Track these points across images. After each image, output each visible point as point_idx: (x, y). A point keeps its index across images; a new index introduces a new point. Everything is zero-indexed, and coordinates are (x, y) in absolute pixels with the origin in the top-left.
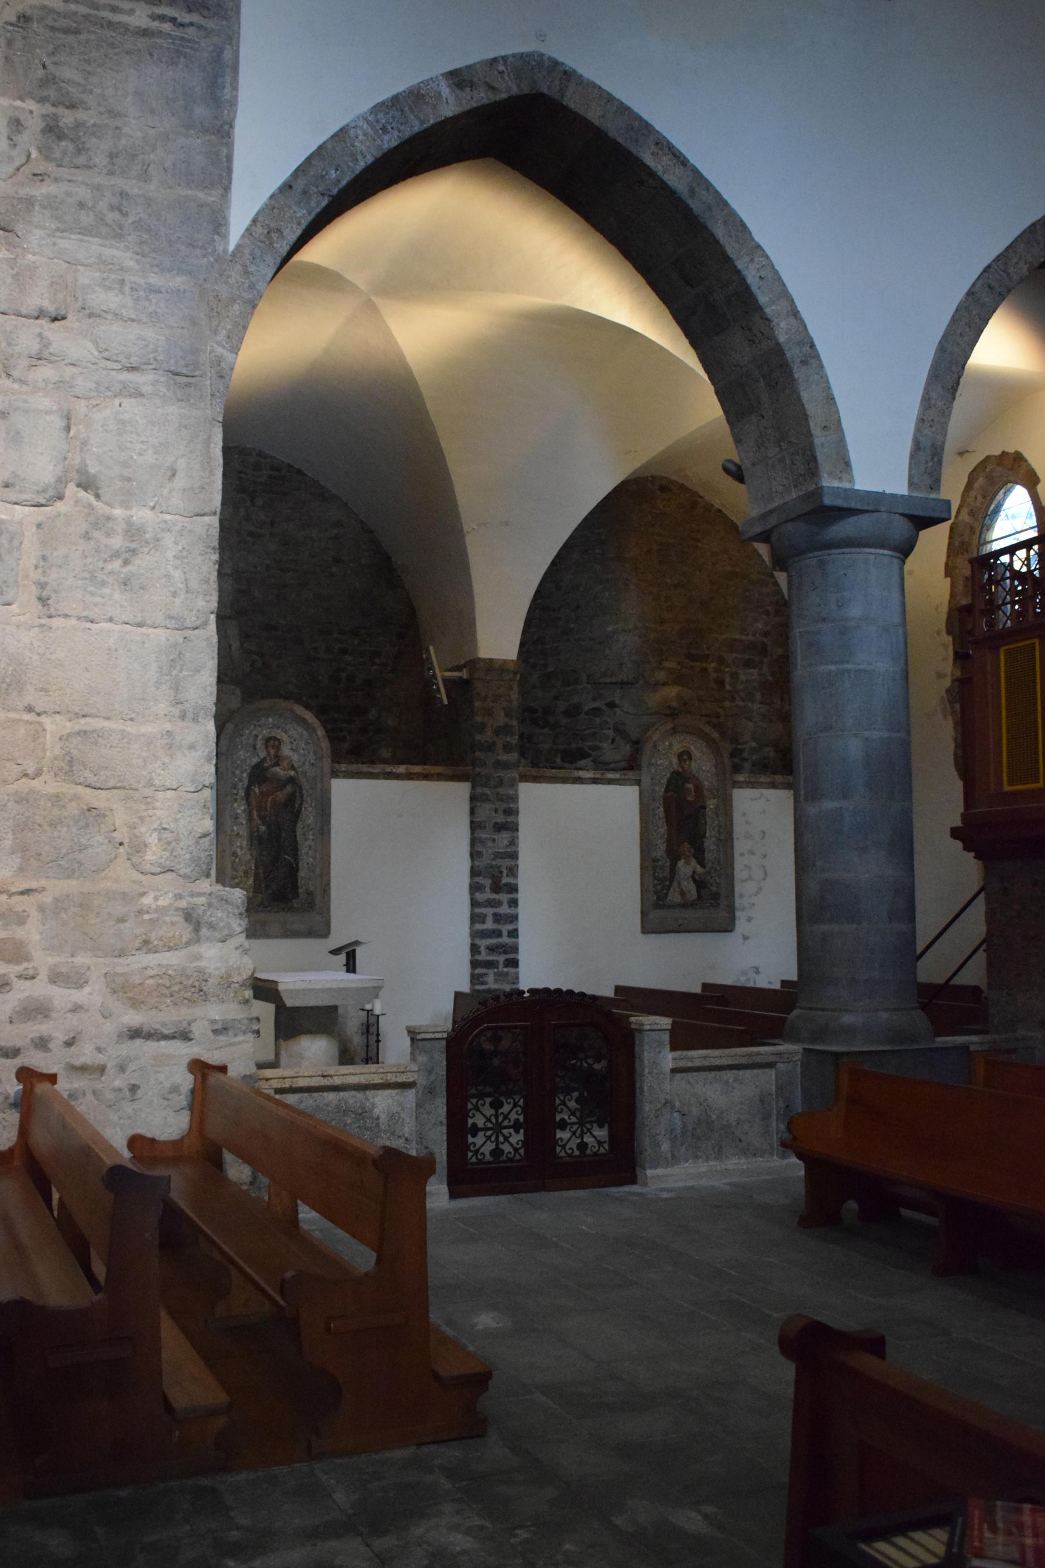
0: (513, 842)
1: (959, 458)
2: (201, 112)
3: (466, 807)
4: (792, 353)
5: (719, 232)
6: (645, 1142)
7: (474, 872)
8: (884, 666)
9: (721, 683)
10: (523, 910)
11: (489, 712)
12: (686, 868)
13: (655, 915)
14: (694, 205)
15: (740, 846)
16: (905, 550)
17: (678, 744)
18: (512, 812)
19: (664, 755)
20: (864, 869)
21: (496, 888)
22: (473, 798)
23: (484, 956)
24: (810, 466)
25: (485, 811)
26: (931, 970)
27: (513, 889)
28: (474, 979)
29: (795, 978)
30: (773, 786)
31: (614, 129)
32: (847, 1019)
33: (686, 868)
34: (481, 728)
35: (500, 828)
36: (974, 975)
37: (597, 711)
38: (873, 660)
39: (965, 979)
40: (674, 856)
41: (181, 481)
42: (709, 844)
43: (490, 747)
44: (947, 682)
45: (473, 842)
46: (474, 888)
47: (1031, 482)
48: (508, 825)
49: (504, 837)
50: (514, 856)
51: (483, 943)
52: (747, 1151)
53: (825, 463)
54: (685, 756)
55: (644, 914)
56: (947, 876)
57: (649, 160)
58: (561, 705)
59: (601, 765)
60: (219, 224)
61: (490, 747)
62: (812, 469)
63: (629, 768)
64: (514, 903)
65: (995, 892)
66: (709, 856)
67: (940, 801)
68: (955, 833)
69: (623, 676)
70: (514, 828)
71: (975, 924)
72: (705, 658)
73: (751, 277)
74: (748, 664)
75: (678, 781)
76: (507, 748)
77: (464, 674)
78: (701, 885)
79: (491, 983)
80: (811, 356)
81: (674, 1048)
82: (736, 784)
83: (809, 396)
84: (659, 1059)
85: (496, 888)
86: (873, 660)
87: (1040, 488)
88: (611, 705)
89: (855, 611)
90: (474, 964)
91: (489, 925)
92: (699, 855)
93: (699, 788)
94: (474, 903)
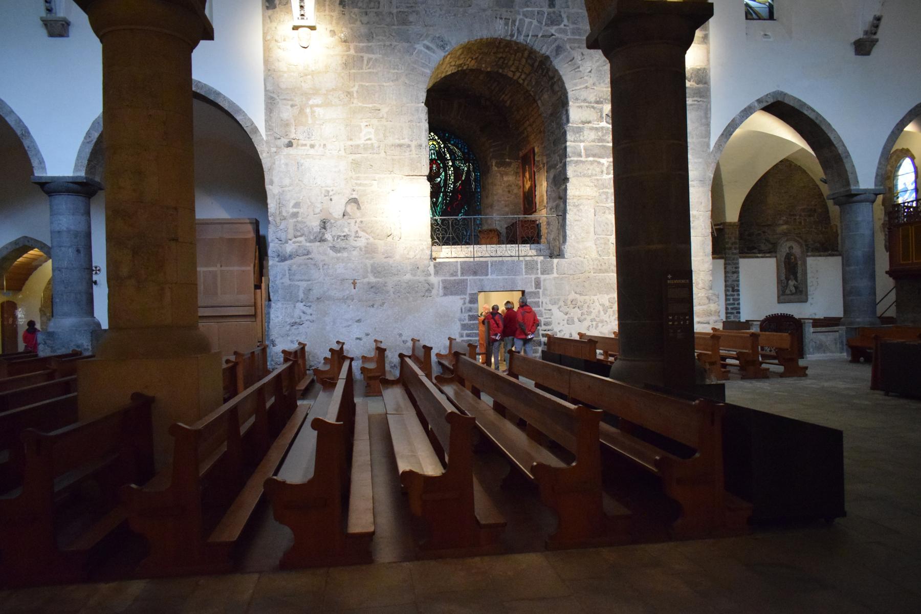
0: (738, 277)
1: (878, 14)
2: (704, 121)
3: (723, 267)
4: (843, 155)
5: (824, 128)
6: (806, 348)
7: (726, 286)
8: (867, 232)
9: (800, 223)
10: (741, 297)
11: (730, 238)
12: (792, 283)
13: (782, 297)
14: (817, 122)
15: (809, 275)
16: (873, 202)
17: (789, 244)
18: (737, 268)
19: (784, 248)
20: (862, 284)
21: (733, 291)
22: (725, 264)
23: (730, 311)
24: (848, 183)
25: (729, 268)
26: (880, 310)
27: (738, 291)
28: (727, 317)
29: (444, 471)
30: (820, 256)
31: (797, 106)
32: (858, 320)
33: (792, 283)
34: (727, 243)
35: (734, 273)
36: (892, 313)
37: (759, 234)
38: (865, 231)
39: (887, 314)
40: (788, 279)
41: (703, 204)
42: (799, 275)
43: (730, 248)
44: (882, 222)
45: (726, 277)
46: (726, 291)
47: (913, 159)
48: (736, 272)
49: (735, 275)
50: (738, 281)
51: (730, 307)
52: (832, 352)
53: (851, 181)
54: (791, 248)
55: (778, 297)
56: (885, 284)
57: (806, 112)
58: (747, 233)
59: (760, 252)
60: (708, 145)
61: (730, 248)
62: (848, 184)
63: (771, 251)
64: (739, 295)
65: (898, 288)
66: (799, 279)
67: (883, 262)
68: (887, 272)
69: (769, 223)
70: (737, 272)
71: (893, 296)
72: (795, 215)
73: (832, 138)
74: (810, 216)
75: (788, 256)
76: (735, 248)
77: (721, 227)
78: (796, 288)
79: (732, 319)
80: (848, 155)
81: (813, 326)
82: (808, 256)
83: (848, 167)
84: (809, 330)
85: (733, 291)
86: (865, 230)
87: (916, 161)
88: (764, 232)
89: (859, 219)
90: (727, 313)
91: (731, 301)
92: (796, 279)
93: (795, 258)
94: (726, 295)
